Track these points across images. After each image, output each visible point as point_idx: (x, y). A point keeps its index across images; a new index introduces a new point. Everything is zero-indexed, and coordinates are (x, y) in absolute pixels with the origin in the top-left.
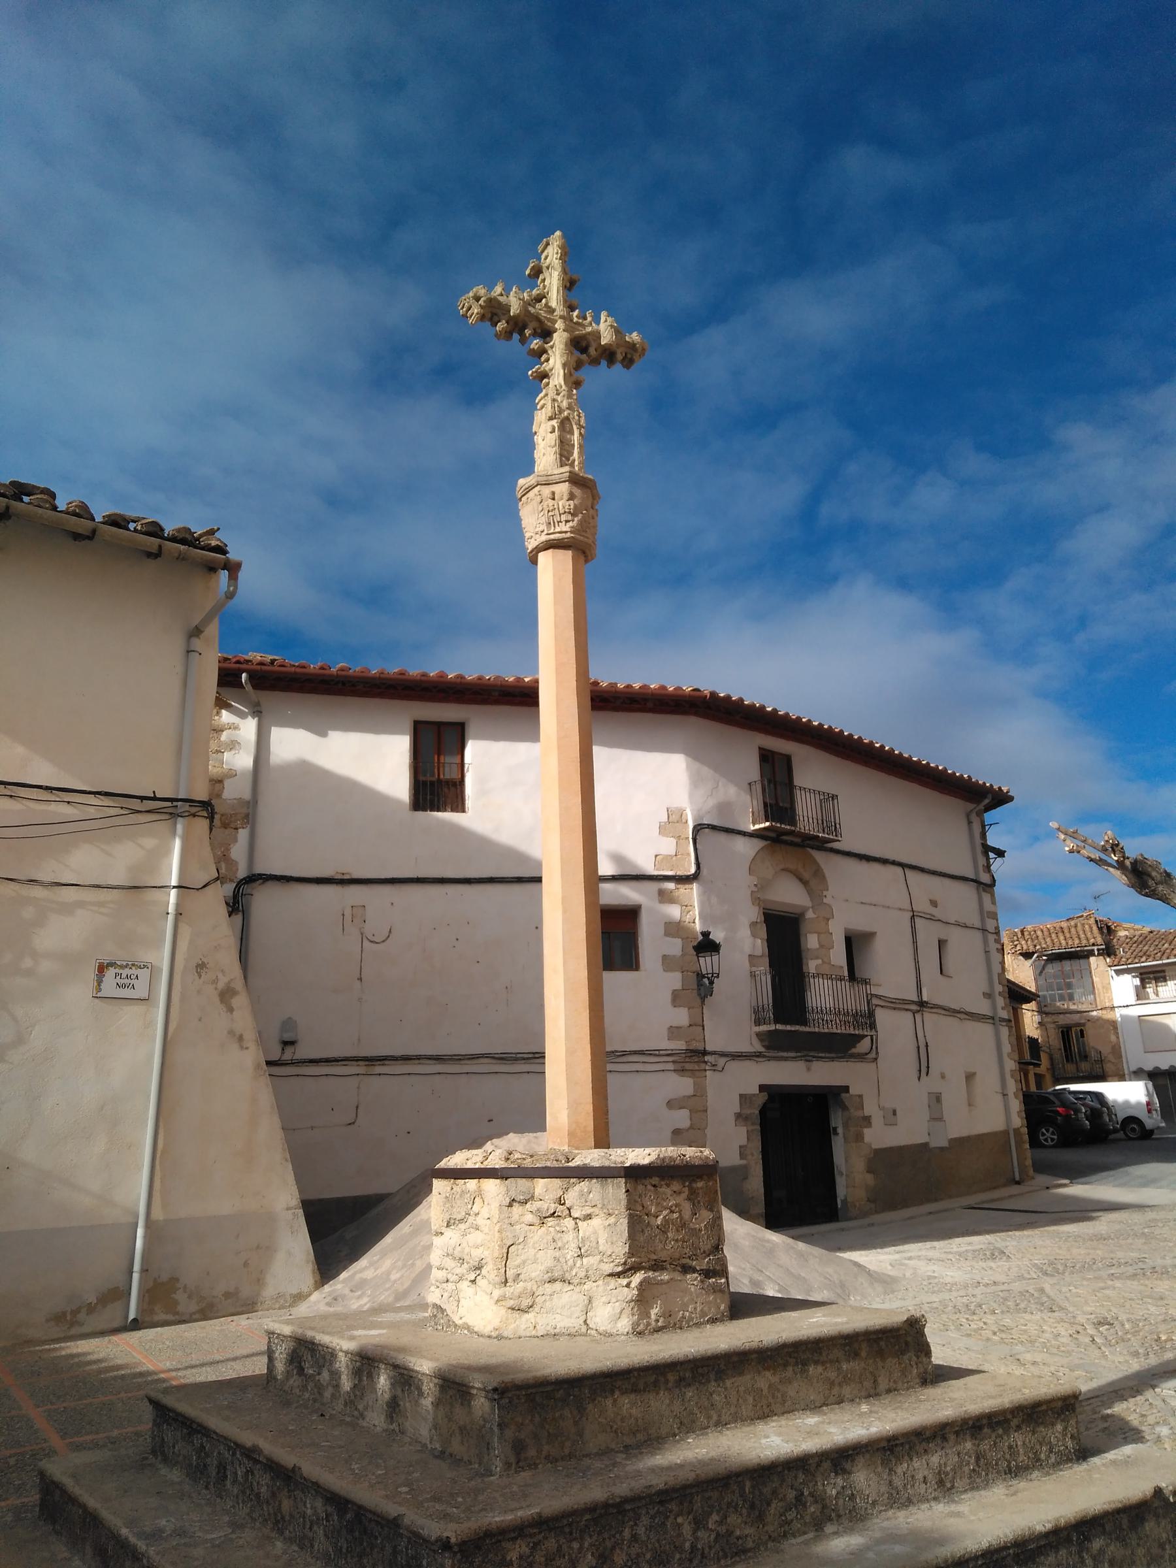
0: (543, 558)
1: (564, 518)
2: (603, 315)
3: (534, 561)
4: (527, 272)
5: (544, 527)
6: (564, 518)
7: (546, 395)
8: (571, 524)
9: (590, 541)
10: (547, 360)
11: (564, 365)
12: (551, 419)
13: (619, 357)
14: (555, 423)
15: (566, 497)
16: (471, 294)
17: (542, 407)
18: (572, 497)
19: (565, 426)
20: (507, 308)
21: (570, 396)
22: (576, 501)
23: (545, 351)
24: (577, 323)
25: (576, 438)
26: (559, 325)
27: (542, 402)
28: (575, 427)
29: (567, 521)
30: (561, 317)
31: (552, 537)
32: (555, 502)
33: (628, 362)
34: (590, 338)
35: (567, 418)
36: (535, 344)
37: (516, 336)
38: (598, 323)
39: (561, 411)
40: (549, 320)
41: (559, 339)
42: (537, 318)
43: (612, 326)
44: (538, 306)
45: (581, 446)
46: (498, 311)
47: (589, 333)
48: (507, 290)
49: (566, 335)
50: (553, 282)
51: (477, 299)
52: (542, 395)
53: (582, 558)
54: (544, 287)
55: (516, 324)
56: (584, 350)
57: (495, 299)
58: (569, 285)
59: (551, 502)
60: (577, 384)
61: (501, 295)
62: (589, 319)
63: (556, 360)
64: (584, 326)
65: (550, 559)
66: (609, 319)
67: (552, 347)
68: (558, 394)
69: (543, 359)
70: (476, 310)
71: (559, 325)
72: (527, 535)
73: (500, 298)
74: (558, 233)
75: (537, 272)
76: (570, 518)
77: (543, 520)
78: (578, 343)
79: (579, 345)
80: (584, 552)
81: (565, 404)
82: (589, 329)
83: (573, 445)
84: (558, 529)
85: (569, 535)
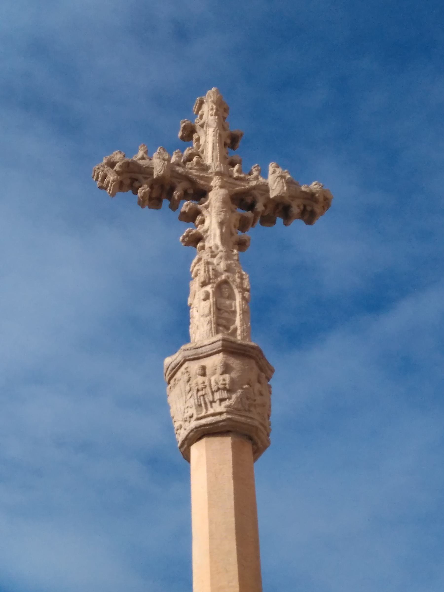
0: (198, 451)
1: (217, 396)
2: (271, 167)
3: (187, 457)
4: (180, 134)
5: (193, 411)
6: (217, 396)
7: (200, 259)
8: (227, 403)
9: (256, 423)
10: (203, 222)
11: (221, 224)
12: (204, 284)
13: (295, 210)
14: (209, 288)
15: (219, 371)
16: (105, 161)
17: (196, 275)
18: (226, 369)
19: (222, 290)
20: (148, 171)
21: (228, 257)
22: (234, 375)
23: (198, 213)
24: (237, 179)
25: (238, 303)
26: (215, 182)
27: (195, 269)
28: (236, 291)
29: (222, 400)
30: (217, 174)
31: (203, 421)
32: (206, 379)
33: (309, 216)
34: (256, 192)
35: (225, 282)
36: (186, 206)
37: (166, 203)
38: (265, 176)
39: (217, 274)
40: (202, 178)
41: (216, 196)
42: (187, 178)
43: (282, 177)
44: (189, 165)
45: (244, 312)
46: (140, 177)
47: (254, 188)
48: (148, 154)
49: (223, 192)
50: (208, 140)
51: (112, 165)
52: (195, 260)
53: (248, 448)
54: (199, 146)
55: (162, 187)
56: (251, 207)
57: (134, 163)
58: (230, 142)
59: (200, 379)
60: (242, 245)
61: (143, 158)
62: (255, 173)
63: (212, 221)
64: (248, 181)
65: (204, 452)
66: (279, 170)
67: (207, 207)
68: (213, 256)
69: (197, 222)
70: (111, 177)
71: (215, 182)
72: (176, 425)
73: (141, 162)
74: (214, 89)
75: (190, 133)
76: (225, 395)
77: (192, 402)
78: (242, 200)
79: (242, 201)
80: (250, 438)
81: (222, 266)
82: (254, 183)
83: (234, 312)
84: (211, 411)
85: (224, 416)
